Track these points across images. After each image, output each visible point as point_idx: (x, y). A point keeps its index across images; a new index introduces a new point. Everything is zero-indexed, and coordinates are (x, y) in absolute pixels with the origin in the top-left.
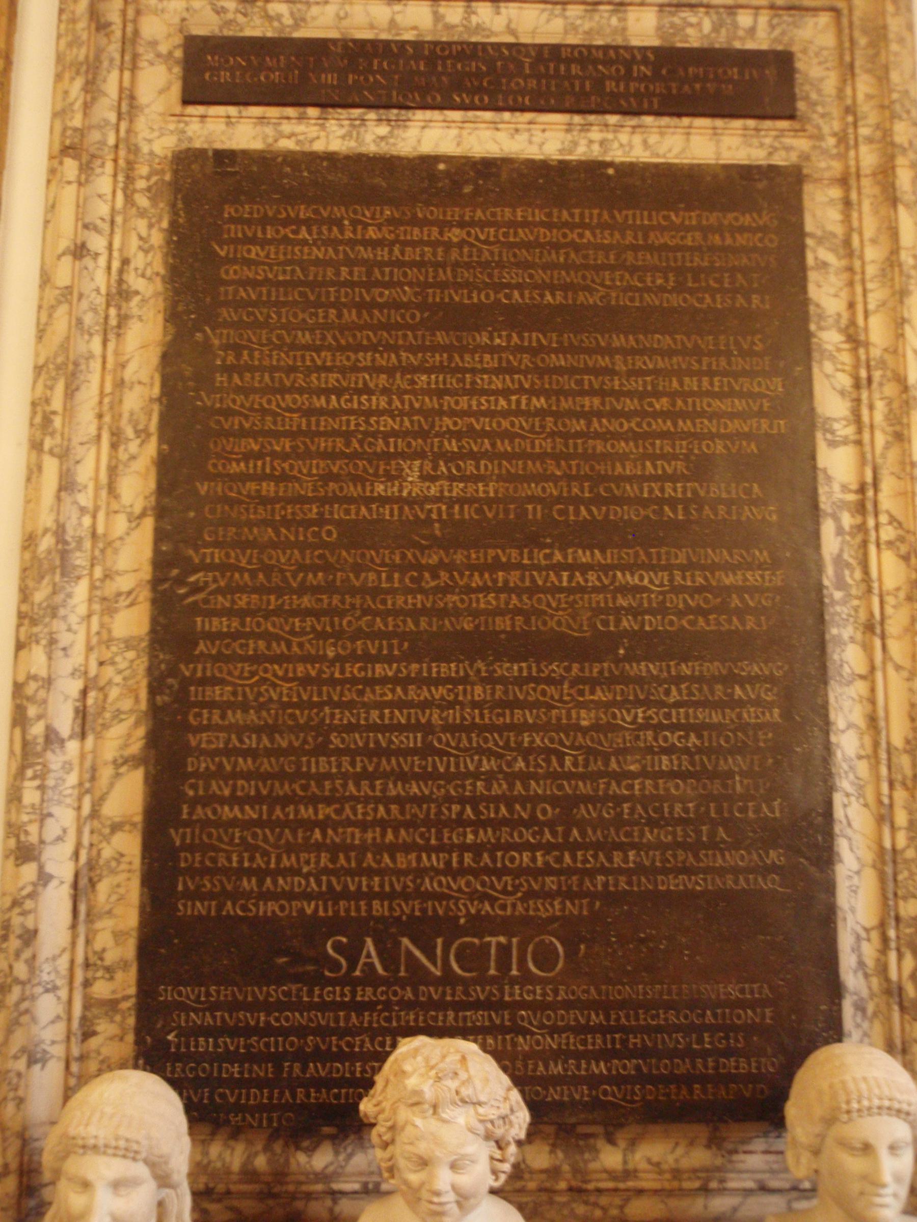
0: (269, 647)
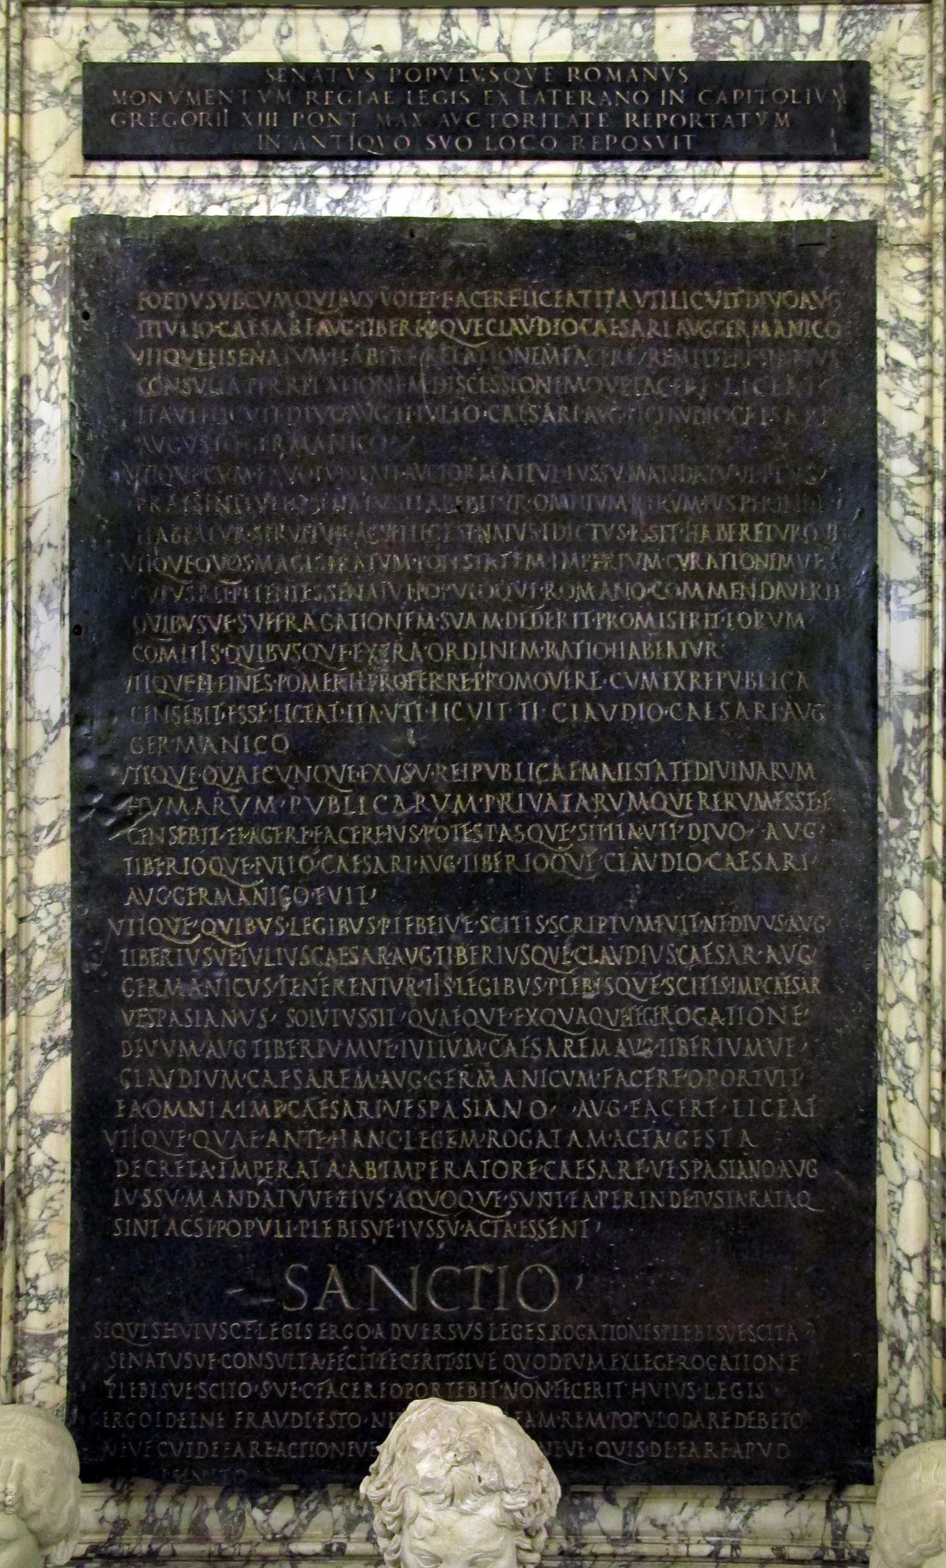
0: (211, 897)
